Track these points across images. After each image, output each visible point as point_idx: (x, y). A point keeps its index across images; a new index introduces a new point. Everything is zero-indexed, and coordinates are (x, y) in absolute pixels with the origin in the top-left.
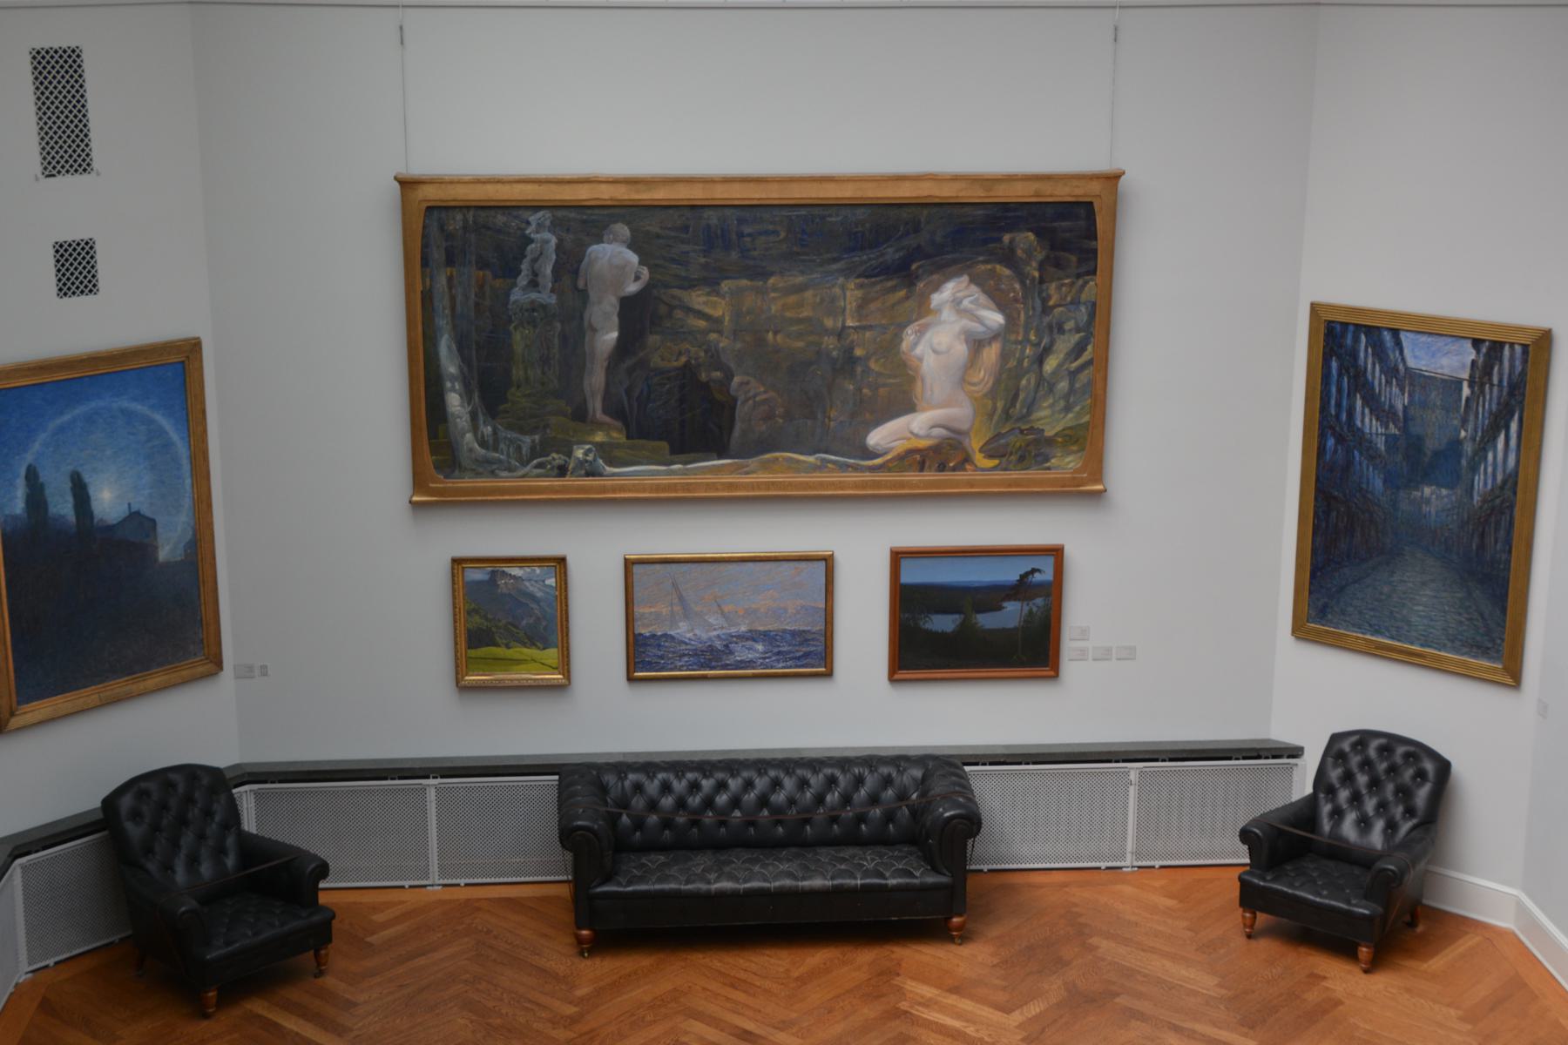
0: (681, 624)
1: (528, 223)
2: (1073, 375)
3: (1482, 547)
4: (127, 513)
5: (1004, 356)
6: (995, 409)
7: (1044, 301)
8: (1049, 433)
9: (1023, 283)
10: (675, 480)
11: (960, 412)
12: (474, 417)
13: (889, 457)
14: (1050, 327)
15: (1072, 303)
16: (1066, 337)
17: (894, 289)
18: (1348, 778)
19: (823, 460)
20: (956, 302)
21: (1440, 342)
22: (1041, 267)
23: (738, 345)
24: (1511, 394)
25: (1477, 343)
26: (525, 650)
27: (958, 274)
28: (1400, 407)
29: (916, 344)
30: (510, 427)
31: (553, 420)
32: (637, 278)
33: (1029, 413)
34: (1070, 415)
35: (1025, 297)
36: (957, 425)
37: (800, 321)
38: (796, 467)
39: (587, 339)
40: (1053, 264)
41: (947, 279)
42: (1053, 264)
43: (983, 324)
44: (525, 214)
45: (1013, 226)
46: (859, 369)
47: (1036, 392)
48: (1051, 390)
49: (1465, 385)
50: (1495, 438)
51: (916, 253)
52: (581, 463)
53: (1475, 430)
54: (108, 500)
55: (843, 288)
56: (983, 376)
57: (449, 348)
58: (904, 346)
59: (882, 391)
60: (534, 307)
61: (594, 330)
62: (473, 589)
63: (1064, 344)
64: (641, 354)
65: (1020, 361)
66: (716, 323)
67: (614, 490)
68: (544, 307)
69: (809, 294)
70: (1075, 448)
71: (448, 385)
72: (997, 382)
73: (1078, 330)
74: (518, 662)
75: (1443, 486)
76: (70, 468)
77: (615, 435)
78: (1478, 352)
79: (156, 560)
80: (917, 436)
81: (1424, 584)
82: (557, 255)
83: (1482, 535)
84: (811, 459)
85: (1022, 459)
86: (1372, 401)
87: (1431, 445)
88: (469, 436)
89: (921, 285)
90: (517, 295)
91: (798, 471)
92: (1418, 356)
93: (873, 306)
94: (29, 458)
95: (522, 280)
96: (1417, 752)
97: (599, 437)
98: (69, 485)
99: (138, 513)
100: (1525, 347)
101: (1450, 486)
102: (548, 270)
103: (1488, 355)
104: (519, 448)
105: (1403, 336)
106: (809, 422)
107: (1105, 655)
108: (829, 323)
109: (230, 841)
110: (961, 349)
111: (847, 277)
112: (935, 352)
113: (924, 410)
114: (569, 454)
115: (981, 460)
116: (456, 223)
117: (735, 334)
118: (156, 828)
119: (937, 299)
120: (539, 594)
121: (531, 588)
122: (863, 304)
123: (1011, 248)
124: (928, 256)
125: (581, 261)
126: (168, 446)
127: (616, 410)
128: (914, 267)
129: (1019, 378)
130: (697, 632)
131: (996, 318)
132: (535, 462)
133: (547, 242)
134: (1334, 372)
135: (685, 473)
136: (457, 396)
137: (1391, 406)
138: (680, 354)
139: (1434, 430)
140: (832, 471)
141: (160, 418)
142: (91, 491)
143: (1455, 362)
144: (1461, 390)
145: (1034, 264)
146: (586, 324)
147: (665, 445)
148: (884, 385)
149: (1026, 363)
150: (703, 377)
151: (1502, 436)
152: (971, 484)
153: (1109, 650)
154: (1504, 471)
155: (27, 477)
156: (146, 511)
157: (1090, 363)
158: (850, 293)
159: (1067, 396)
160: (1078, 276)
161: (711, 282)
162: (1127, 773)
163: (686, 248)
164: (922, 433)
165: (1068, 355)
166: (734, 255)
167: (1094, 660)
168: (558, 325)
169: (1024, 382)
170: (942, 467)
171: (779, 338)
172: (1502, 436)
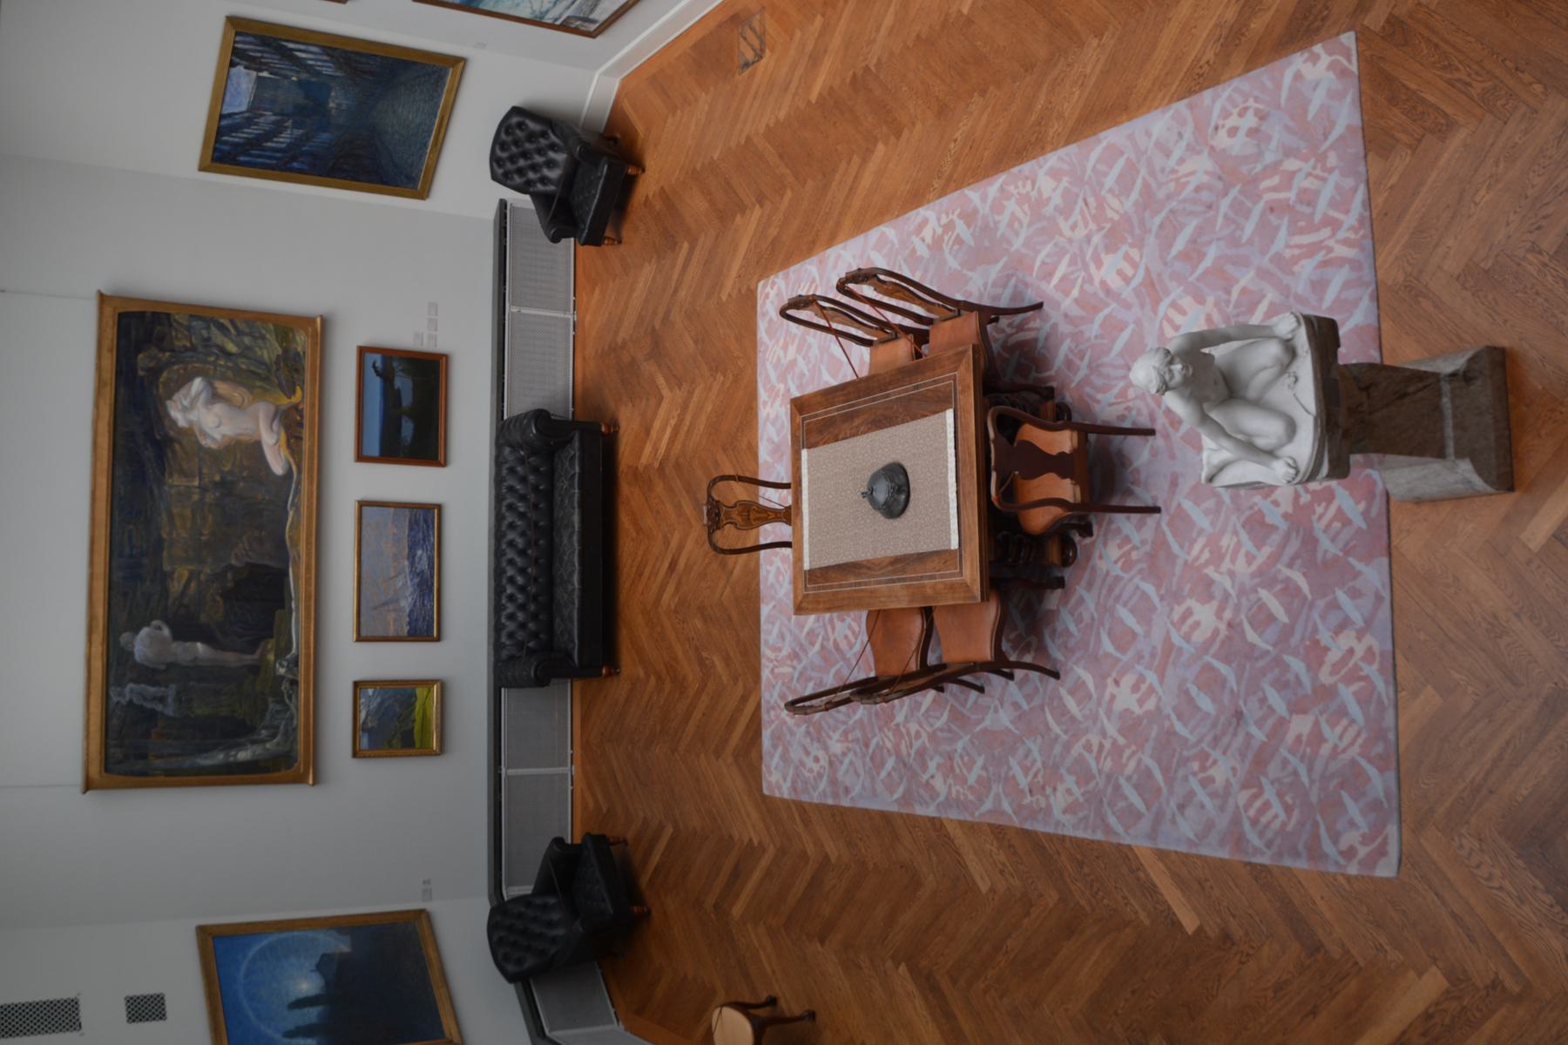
0: (402, 605)
1: (118, 703)
2: (240, 333)
5: (224, 379)
6: (261, 387)
7: (186, 349)
8: (280, 351)
9: (174, 363)
12: (254, 742)
13: (291, 460)
14: (206, 346)
17: (174, 452)
18: (520, 172)
20: (185, 410)
22: (163, 350)
25: (232, 65)
27: (165, 407)
28: (273, 118)
29: (213, 439)
32: (159, 628)
33: (265, 364)
34: (268, 336)
38: (295, 525)
41: (168, 415)
46: (229, 478)
48: (248, 348)
52: (289, 669)
54: (308, 985)
55: (171, 486)
56: (238, 394)
58: (214, 446)
59: (245, 463)
60: (178, 699)
61: (196, 659)
62: (374, 745)
65: (228, 368)
67: (308, 648)
69: (175, 511)
70: (291, 335)
71: (231, 759)
77: (269, 646)
80: (277, 441)
84: (291, 513)
85: (297, 371)
88: (268, 745)
89: (172, 433)
90: (170, 711)
92: (240, 101)
94: (278, 1036)
95: (159, 708)
96: (505, 126)
97: (271, 657)
102: (152, 690)
104: (278, 712)
105: (225, 112)
107: (433, 323)
108: (196, 497)
109: (538, 901)
110: (218, 408)
112: (219, 426)
113: (260, 435)
114: (282, 678)
115: (296, 399)
119: (182, 423)
120: (379, 700)
121: (374, 705)
123: (149, 370)
127: (253, 646)
128: (158, 437)
131: (197, 384)
132: (287, 701)
140: (299, 500)
141: (252, 953)
142: (301, 996)
145: (160, 355)
149: (230, 364)
150: (230, 585)
152: (313, 406)
153: (430, 321)
156: (316, 960)
157: (232, 322)
158: (176, 481)
159: (255, 338)
160: (171, 325)
161: (163, 578)
165: (226, 336)
166: (146, 561)
168: (191, 683)
169: (243, 366)
170: (301, 425)
171: (205, 532)
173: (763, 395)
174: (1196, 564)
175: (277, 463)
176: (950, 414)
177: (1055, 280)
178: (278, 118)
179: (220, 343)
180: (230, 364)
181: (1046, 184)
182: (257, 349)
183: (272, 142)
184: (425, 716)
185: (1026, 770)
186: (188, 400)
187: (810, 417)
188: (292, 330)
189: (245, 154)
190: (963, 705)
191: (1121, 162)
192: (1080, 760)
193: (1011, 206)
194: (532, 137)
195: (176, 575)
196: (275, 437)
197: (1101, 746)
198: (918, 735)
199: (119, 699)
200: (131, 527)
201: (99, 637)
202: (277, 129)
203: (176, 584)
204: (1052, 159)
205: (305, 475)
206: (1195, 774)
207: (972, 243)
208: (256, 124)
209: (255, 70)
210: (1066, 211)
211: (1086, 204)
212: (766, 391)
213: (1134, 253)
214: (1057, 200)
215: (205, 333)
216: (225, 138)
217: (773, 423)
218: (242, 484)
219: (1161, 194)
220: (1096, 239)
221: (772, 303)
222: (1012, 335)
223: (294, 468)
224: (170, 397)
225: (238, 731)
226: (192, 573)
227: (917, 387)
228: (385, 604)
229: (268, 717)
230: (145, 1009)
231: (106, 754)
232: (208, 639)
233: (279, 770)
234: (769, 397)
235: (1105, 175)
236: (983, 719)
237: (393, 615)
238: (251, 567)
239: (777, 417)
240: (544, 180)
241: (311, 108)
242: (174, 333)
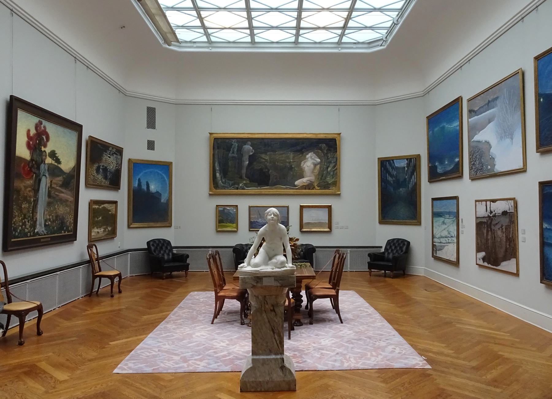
0: (259, 219)
1: (232, 141)
2: (334, 171)
4: (156, 191)
5: (320, 168)
6: (319, 178)
7: (328, 157)
8: (329, 182)
11: (312, 178)
12: (221, 177)
13: (299, 187)
14: (329, 162)
15: (333, 157)
16: (332, 164)
17: (299, 154)
18: (391, 247)
19: (286, 187)
20: (311, 157)
23: (270, 165)
25: (407, 159)
26: (229, 224)
27: (311, 152)
28: (395, 174)
29: (303, 165)
30: (228, 180)
33: (326, 179)
34: (333, 179)
35: (324, 156)
37: (282, 160)
39: (243, 163)
40: (329, 150)
41: (309, 153)
42: (329, 150)
43: (316, 161)
44: (232, 140)
46: (293, 169)
48: (330, 174)
49: (406, 168)
50: (411, 179)
52: (241, 187)
53: (408, 176)
54: (153, 188)
55: (290, 154)
56: (317, 171)
57: (217, 165)
58: (302, 165)
60: (233, 157)
61: (244, 161)
62: (220, 211)
63: (332, 165)
68: (235, 157)
69: (283, 155)
70: (334, 185)
71: (217, 171)
74: (229, 226)
75: (403, 188)
76: (146, 180)
77: (247, 181)
78: (408, 161)
79: (161, 201)
80: (304, 183)
82: (238, 147)
84: (284, 187)
85: (324, 187)
88: (220, 181)
89: (304, 154)
90: (230, 155)
92: (398, 164)
94: (139, 177)
95: (231, 152)
96: (403, 241)
97: (244, 182)
98: (146, 183)
99: (158, 192)
100: (416, 158)
104: (230, 184)
105: (395, 161)
107: (342, 228)
109: (171, 254)
110: (312, 166)
112: (308, 166)
114: (239, 185)
115: (316, 187)
116: (219, 141)
118: (156, 248)
119: (307, 156)
120: (232, 213)
121: (231, 211)
122: (293, 158)
124: (305, 148)
125: (242, 148)
126: (165, 181)
129: (324, 171)
130: (263, 221)
131: (319, 160)
132: (232, 187)
134: (383, 170)
136: (218, 174)
137: (393, 174)
138: (260, 166)
140: (288, 189)
141: (163, 175)
142: (150, 186)
144: (405, 169)
145: (326, 150)
148: (298, 172)
150: (264, 171)
151: (413, 176)
153: (343, 227)
154: (414, 182)
155: (138, 180)
156: (160, 192)
157: (337, 169)
158: (291, 155)
159: (332, 176)
160: (334, 152)
161: (265, 153)
162: (347, 251)
163: (261, 146)
164: (305, 182)
166: (270, 148)
167: (340, 228)
168: (237, 161)
169: (324, 172)
170: (309, 189)
171: (278, 163)
172: (413, 176)
178: (395, 175)
179: (330, 166)
182: (329, 176)
183: (388, 175)
184: (227, 227)
189: (384, 169)
194: (401, 248)
195: (266, 156)
199: (233, 142)
200: (279, 144)
201: (250, 136)
202: (392, 176)
203: (264, 156)
205: (295, 190)
208: (392, 170)
209: (407, 166)
215: (333, 162)
216: (387, 163)
223: (297, 187)
225: (225, 173)
226: (267, 160)
228: (260, 214)
230: (151, 145)
232: (249, 164)
233: (213, 185)
237: (256, 216)
238: (269, 176)
240: (389, 253)
241: (399, 184)
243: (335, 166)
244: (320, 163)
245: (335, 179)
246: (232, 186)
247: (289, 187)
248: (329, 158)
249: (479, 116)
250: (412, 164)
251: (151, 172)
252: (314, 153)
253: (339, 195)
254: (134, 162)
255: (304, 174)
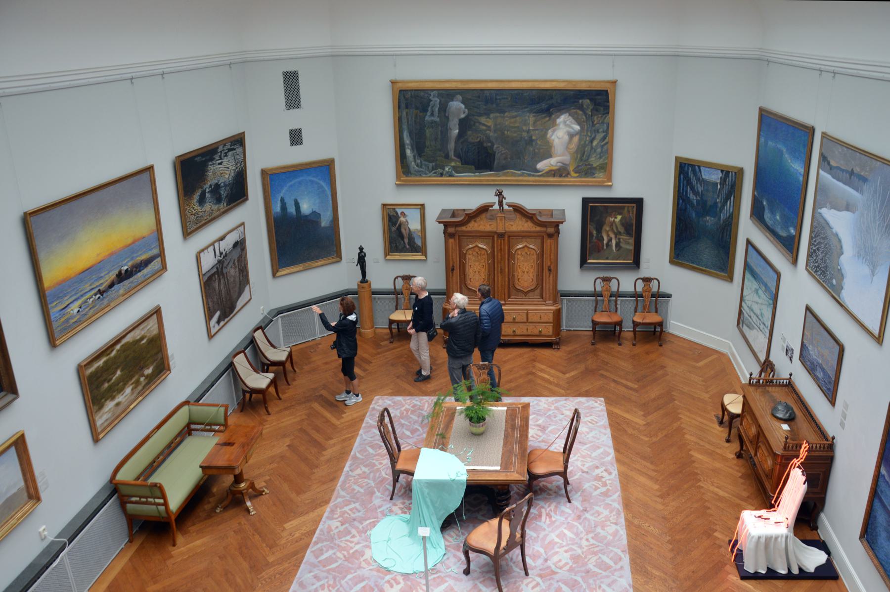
2: (602, 147)
3: (723, 237)
5: (580, 140)
7: (593, 122)
8: (595, 165)
9: (586, 116)
10: (477, 178)
11: (567, 158)
12: (414, 157)
13: (544, 172)
14: (595, 131)
17: (545, 117)
20: (565, 122)
21: (712, 170)
22: (592, 111)
23: (496, 135)
24: (731, 188)
25: (722, 171)
28: (700, 191)
29: (552, 135)
30: (425, 160)
31: (438, 158)
32: (464, 113)
33: (588, 159)
34: (601, 160)
35: (587, 121)
36: (564, 162)
37: (515, 127)
38: (514, 175)
40: (595, 110)
41: (562, 114)
42: (595, 110)
44: (429, 92)
45: (582, 98)
46: (534, 143)
47: (590, 152)
48: (595, 151)
50: (727, 202)
51: (551, 106)
52: (448, 172)
54: (306, 208)
55: (529, 117)
58: (548, 136)
59: (541, 150)
60: (432, 122)
63: (600, 136)
64: (466, 137)
65: (585, 142)
66: (489, 128)
67: (457, 181)
68: (435, 122)
69: (518, 118)
71: (407, 147)
72: (578, 149)
73: (604, 132)
77: (458, 163)
78: (722, 174)
79: (321, 226)
80: (552, 165)
81: (706, 248)
83: (723, 233)
84: (519, 172)
85: (586, 174)
86: (692, 189)
87: (709, 203)
88: (413, 163)
89: (553, 116)
90: (427, 118)
91: (515, 176)
93: (538, 123)
94: (282, 195)
95: (429, 113)
97: (453, 164)
99: (315, 212)
100: (735, 173)
101: (714, 217)
102: (437, 110)
103: (725, 175)
104: (428, 168)
105: (701, 168)
106: (519, 161)
108: (524, 128)
110: (566, 137)
111: (530, 113)
112: (558, 138)
113: (555, 157)
114: (444, 169)
116: (409, 95)
117: (495, 131)
119: (558, 121)
123: (582, 105)
124: (556, 107)
125: (446, 107)
126: (324, 191)
127: (458, 156)
128: (551, 110)
132: (433, 172)
133: (436, 101)
135: (480, 176)
137: (698, 191)
138: (478, 137)
139: (710, 198)
142: (301, 205)
143: (715, 177)
145: (590, 110)
146: (448, 127)
147: (473, 167)
149: (587, 142)
150: (485, 145)
152: (570, 182)
155: (281, 201)
156: (317, 211)
157: (607, 143)
158: (531, 118)
159: (600, 154)
160: (604, 114)
161: (487, 114)
163: (480, 103)
165: (600, 140)
166: (494, 106)
168: (440, 128)
169: (586, 149)
170: (561, 176)
173: (551, 399)
174: (418, 588)
175: (542, 165)
176: (498, 468)
177: (566, 531)
180: (587, 142)
181: (612, 528)
185: (351, 510)
186: (569, 123)
187: (519, 411)
188: (605, 171)
190: (388, 484)
191: (611, 563)
192: (349, 533)
193: (606, 513)
195: (488, 120)
196: (554, 164)
197: (352, 542)
198: (381, 464)
199: (432, 96)
200: (509, 99)
203: (485, 120)
204: (623, 533)
205: (537, 178)
206: (327, 582)
207: (593, 495)
210: (596, 537)
211: (596, 547)
212: (552, 401)
213: (567, 567)
214: (603, 533)
217: (537, 404)
218: (532, 149)
219: (591, 581)
220: (579, 551)
221: (593, 404)
222: (546, 511)
223: (540, 173)
224: (570, 115)
225: (419, 149)
226: (489, 127)
227: (515, 456)
229: (427, 163)
230: (296, 137)
231: (407, 90)
232: (460, 135)
234: (549, 402)
235: (608, 557)
236: (379, 492)
239: (540, 405)
241: (706, 209)
242: (600, 116)
243: (605, 138)
244: (579, 133)
245: (604, 160)
246: (432, 170)
247: (527, 174)
248: (596, 124)
249: (834, 181)
250: (729, 180)
251: (300, 183)
252: (570, 115)
253: (610, 186)
254: (270, 172)
255: (553, 151)
